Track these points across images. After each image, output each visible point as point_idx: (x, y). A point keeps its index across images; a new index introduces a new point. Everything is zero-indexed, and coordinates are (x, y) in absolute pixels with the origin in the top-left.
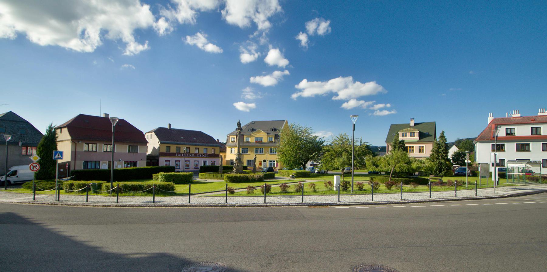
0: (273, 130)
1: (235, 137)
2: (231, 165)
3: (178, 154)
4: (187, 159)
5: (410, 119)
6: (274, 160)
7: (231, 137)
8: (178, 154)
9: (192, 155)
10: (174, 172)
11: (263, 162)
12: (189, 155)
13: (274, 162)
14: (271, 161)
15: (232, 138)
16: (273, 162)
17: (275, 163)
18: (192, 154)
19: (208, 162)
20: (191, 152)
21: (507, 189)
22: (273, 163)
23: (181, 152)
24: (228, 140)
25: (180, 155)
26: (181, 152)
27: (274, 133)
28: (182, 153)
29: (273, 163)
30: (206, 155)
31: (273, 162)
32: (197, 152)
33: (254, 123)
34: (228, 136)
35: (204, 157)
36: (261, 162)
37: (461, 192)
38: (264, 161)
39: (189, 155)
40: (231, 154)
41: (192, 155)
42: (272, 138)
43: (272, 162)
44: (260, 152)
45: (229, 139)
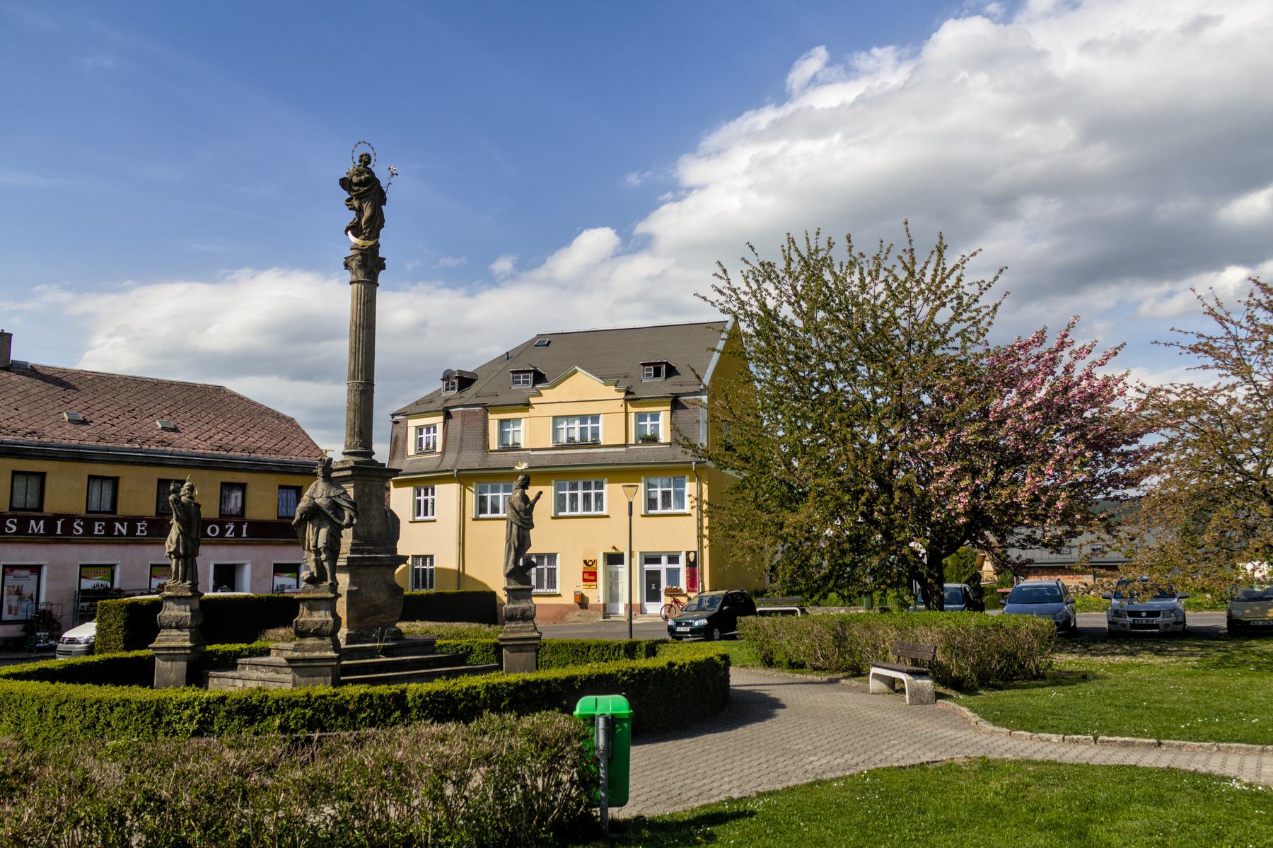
0: (657, 374)
1: (438, 420)
2: (417, 586)
3: (23, 524)
4: (97, 554)
5: (349, 248)
6: (672, 548)
7: (413, 423)
8: (23, 524)
9: (132, 530)
10: (466, 665)
11: (600, 568)
12: (109, 529)
13: (673, 559)
14: (652, 559)
15: (420, 429)
16: (664, 559)
17: (682, 565)
18: (132, 521)
19: (247, 571)
20: (122, 510)
21: (1084, 677)
22: (663, 567)
23: (49, 508)
24: (400, 443)
25: (38, 527)
26: (49, 508)
27: (665, 386)
28: (58, 516)
29: (663, 567)
30: (238, 531)
31: (664, 559)
32: (32, 501)
33: (544, 342)
34: (396, 422)
35: (88, 537)
36: (594, 562)
37: (1200, 746)
38: (614, 559)
39: (109, 529)
40: (556, 517)
41: (132, 530)
42: (655, 416)
43: (657, 560)
44: (587, 506)
45: (401, 436)
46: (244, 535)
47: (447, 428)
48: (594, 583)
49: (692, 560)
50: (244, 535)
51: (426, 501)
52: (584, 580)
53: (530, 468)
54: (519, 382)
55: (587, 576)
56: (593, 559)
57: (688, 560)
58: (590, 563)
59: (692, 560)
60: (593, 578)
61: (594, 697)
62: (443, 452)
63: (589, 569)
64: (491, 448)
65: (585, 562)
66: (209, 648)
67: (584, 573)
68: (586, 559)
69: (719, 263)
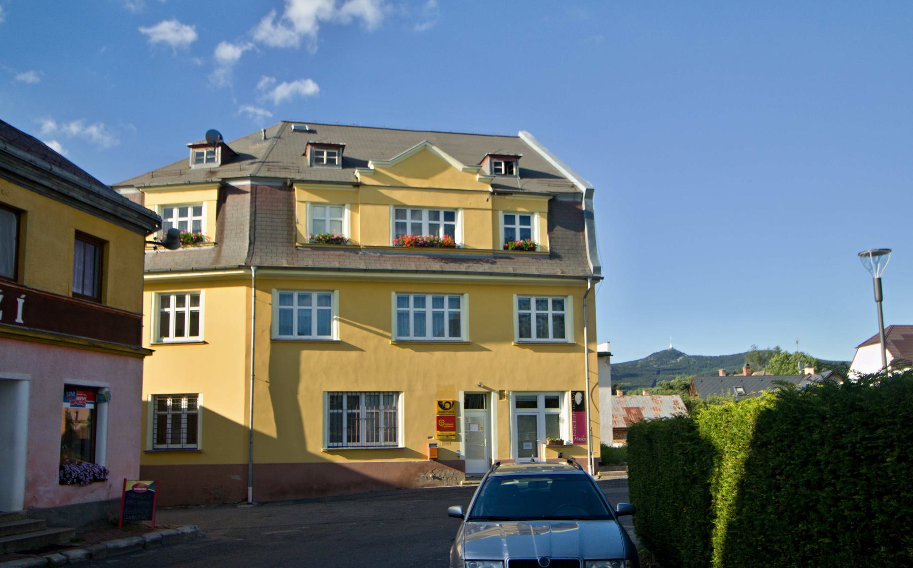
6: (551, 387)
13: (553, 402)
29: (541, 411)
38: (475, 401)
46: (19, 320)
47: (224, 218)
48: (453, 433)
49: (578, 402)
50: (19, 320)
51: (180, 316)
52: (439, 428)
53: (375, 404)
54: (377, 413)
55: (443, 423)
56: (450, 399)
57: (574, 402)
58: (448, 406)
59: (578, 402)
60: (450, 425)
61: (297, 203)
62: (218, 243)
63: (447, 414)
64: (146, 268)
65: (440, 404)
66: (435, 148)
67: (438, 418)
68: (441, 400)
69: (205, 343)
